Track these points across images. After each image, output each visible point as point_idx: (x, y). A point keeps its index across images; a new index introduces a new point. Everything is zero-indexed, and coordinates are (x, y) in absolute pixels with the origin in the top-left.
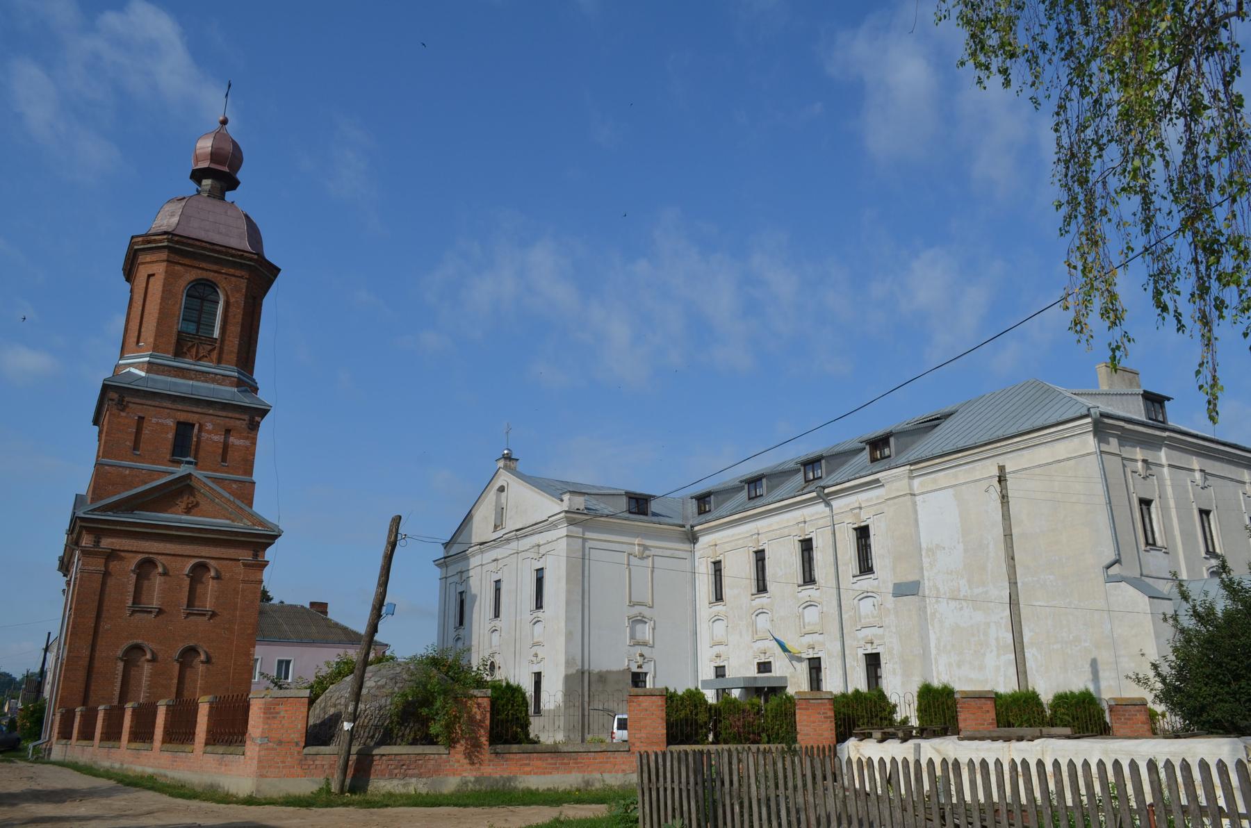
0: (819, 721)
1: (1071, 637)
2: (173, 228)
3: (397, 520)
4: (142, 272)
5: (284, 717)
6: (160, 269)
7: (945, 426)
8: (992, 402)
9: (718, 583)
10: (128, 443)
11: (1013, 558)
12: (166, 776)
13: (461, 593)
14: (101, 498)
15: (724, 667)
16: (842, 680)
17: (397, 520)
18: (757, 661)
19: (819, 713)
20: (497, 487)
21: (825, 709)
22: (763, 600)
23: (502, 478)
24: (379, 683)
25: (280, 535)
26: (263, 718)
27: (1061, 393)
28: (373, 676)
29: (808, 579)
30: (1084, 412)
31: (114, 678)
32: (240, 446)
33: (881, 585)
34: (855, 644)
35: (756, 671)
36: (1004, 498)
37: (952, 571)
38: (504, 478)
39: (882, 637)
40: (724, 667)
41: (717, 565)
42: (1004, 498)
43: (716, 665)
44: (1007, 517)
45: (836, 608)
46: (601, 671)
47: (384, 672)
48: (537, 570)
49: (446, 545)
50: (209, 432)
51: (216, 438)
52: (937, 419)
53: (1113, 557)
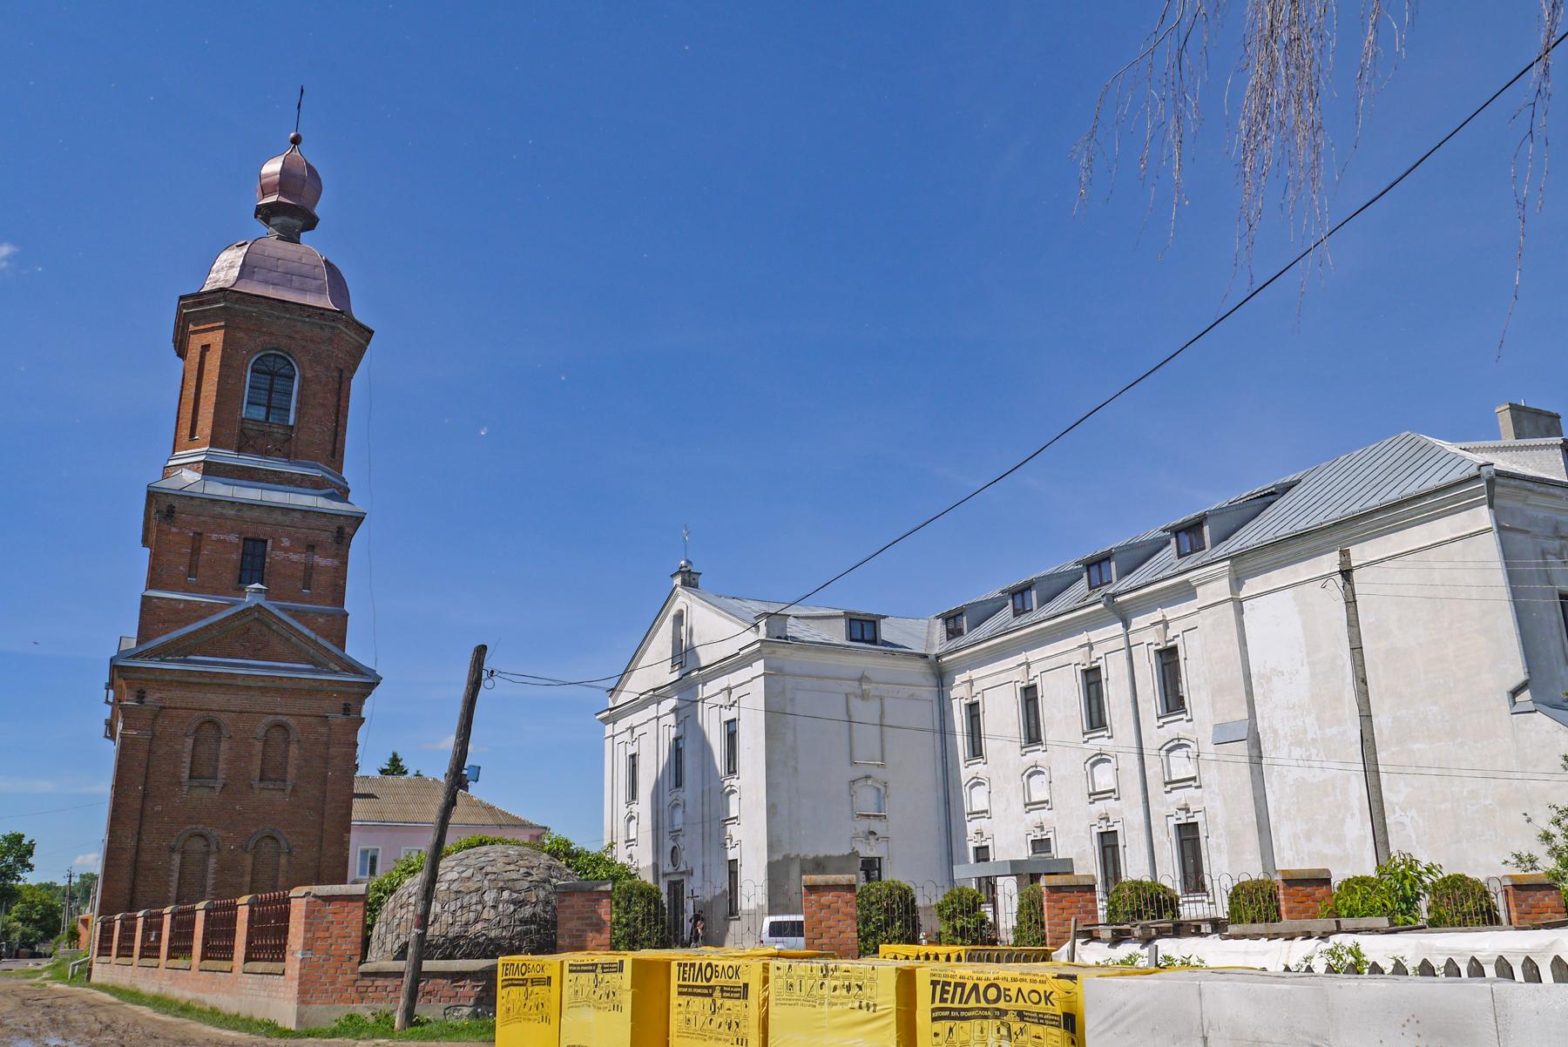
1: (1465, 793)
2: (232, 283)
3: (481, 651)
4: (196, 343)
5: (332, 922)
6: (216, 338)
7: (1281, 504)
8: (1347, 467)
10: (182, 568)
11: (1364, 681)
12: (204, 1003)
13: (633, 756)
14: (149, 639)
15: (987, 847)
16: (1147, 861)
17: (481, 651)
18: (1031, 838)
20: (673, 612)
22: (1036, 756)
23: (680, 599)
24: (463, 875)
25: (378, 684)
26: (305, 923)
27: (1443, 448)
28: (457, 865)
29: (1095, 723)
30: (1473, 471)
31: (169, 876)
32: (327, 567)
33: (1196, 728)
34: (1165, 811)
35: (1030, 852)
36: (1351, 603)
37: (1294, 706)
38: (684, 600)
39: (1201, 800)
40: (987, 847)
42: (1351, 603)
44: (1354, 623)
47: (471, 861)
48: (728, 723)
50: (286, 550)
51: (294, 557)
52: (1272, 493)
53: (1521, 676)
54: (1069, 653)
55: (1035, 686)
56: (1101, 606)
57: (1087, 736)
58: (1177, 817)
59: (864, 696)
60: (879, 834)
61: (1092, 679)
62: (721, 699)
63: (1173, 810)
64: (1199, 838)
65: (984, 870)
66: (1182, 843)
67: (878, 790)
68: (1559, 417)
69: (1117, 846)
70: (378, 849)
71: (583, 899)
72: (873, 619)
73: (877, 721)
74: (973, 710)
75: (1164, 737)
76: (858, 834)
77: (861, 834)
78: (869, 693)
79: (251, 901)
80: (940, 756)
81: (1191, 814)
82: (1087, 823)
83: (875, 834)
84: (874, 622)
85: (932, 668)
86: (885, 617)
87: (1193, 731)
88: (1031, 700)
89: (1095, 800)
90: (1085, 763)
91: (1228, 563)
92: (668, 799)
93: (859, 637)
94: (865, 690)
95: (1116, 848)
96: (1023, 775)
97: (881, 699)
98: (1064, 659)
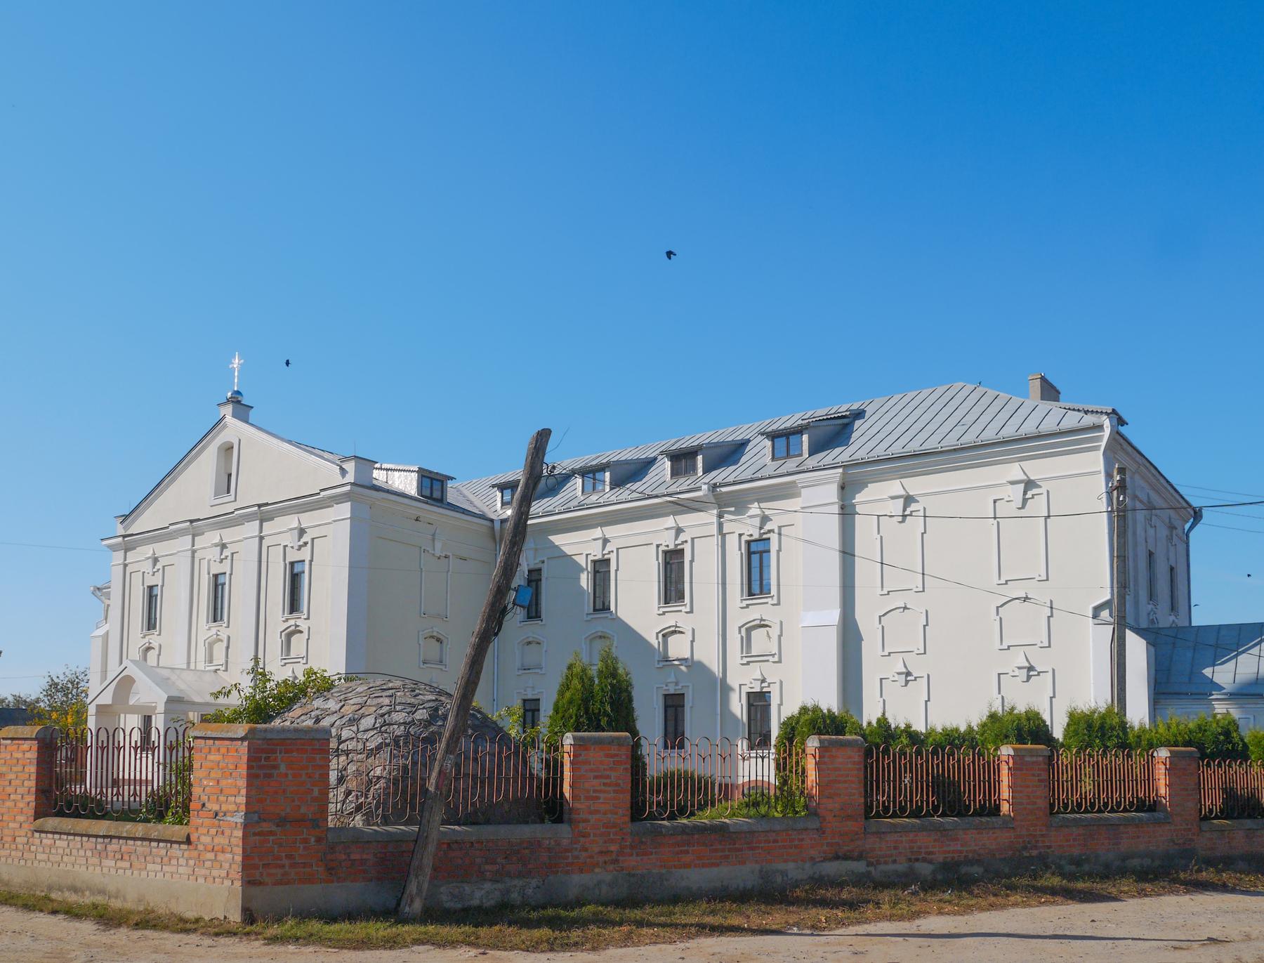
38: (234, 429)
54: (660, 532)
61: (673, 562)
68: (1060, 393)
71: (602, 753)
72: (441, 478)
73: (921, 572)
79: (41, 736)
84: (442, 482)
86: (452, 478)
89: (286, 664)
90: (281, 632)
91: (840, 470)
95: (679, 709)
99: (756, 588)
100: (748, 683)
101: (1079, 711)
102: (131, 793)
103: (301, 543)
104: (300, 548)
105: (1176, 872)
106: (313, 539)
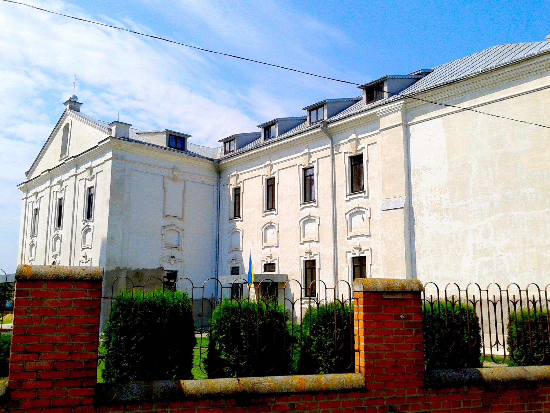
0: (397, 332)
9: (237, 211)
15: (275, 264)
19: (397, 317)
21: (407, 310)
22: (271, 217)
23: (68, 117)
35: (263, 270)
37: (435, 189)
41: (237, 190)
43: (233, 266)
45: (331, 221)
46: (138, 269)
49: (27, 173)
55: (274, 178)
56: (320, 130)
57: (302, 206)
58: (354, 252)
59: (174, 179)
60: (177, 257)
62: (86, 175)
63: (351, 249)
64: (365, 265)
65: (235, 279)
66: (306, 269)
67: (179, 232)
69: (315, 268)
70: (264, 272)
74: (237, 192)
75: (349, 207)
76: (164, 257)
77: (166, 257)
78: (177, 178)
80: (216, 217)
81: (362, 251)
82: (298, 255)
83: (174, 257)
85: (215, 167)
86: (190, 136)
87: (368, 204)
88: (270, 186)
90: (300, 221)
92: (53, 234)
93: (174, 146)
94: (175, 175)
96: (262, 227)
97: (184, 181)
98: (292, 162)
99: (270, 207)
100: (304, 255)
101: (74, 276)
102: (493, 343)
103: (92, 176)
104: (92, 178)
105: (521, 327)
106: (318, 159)
